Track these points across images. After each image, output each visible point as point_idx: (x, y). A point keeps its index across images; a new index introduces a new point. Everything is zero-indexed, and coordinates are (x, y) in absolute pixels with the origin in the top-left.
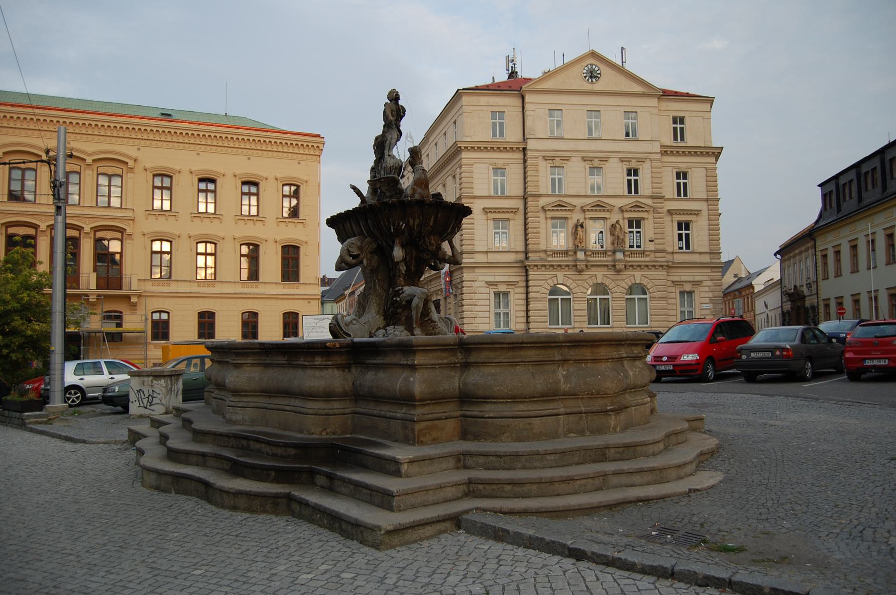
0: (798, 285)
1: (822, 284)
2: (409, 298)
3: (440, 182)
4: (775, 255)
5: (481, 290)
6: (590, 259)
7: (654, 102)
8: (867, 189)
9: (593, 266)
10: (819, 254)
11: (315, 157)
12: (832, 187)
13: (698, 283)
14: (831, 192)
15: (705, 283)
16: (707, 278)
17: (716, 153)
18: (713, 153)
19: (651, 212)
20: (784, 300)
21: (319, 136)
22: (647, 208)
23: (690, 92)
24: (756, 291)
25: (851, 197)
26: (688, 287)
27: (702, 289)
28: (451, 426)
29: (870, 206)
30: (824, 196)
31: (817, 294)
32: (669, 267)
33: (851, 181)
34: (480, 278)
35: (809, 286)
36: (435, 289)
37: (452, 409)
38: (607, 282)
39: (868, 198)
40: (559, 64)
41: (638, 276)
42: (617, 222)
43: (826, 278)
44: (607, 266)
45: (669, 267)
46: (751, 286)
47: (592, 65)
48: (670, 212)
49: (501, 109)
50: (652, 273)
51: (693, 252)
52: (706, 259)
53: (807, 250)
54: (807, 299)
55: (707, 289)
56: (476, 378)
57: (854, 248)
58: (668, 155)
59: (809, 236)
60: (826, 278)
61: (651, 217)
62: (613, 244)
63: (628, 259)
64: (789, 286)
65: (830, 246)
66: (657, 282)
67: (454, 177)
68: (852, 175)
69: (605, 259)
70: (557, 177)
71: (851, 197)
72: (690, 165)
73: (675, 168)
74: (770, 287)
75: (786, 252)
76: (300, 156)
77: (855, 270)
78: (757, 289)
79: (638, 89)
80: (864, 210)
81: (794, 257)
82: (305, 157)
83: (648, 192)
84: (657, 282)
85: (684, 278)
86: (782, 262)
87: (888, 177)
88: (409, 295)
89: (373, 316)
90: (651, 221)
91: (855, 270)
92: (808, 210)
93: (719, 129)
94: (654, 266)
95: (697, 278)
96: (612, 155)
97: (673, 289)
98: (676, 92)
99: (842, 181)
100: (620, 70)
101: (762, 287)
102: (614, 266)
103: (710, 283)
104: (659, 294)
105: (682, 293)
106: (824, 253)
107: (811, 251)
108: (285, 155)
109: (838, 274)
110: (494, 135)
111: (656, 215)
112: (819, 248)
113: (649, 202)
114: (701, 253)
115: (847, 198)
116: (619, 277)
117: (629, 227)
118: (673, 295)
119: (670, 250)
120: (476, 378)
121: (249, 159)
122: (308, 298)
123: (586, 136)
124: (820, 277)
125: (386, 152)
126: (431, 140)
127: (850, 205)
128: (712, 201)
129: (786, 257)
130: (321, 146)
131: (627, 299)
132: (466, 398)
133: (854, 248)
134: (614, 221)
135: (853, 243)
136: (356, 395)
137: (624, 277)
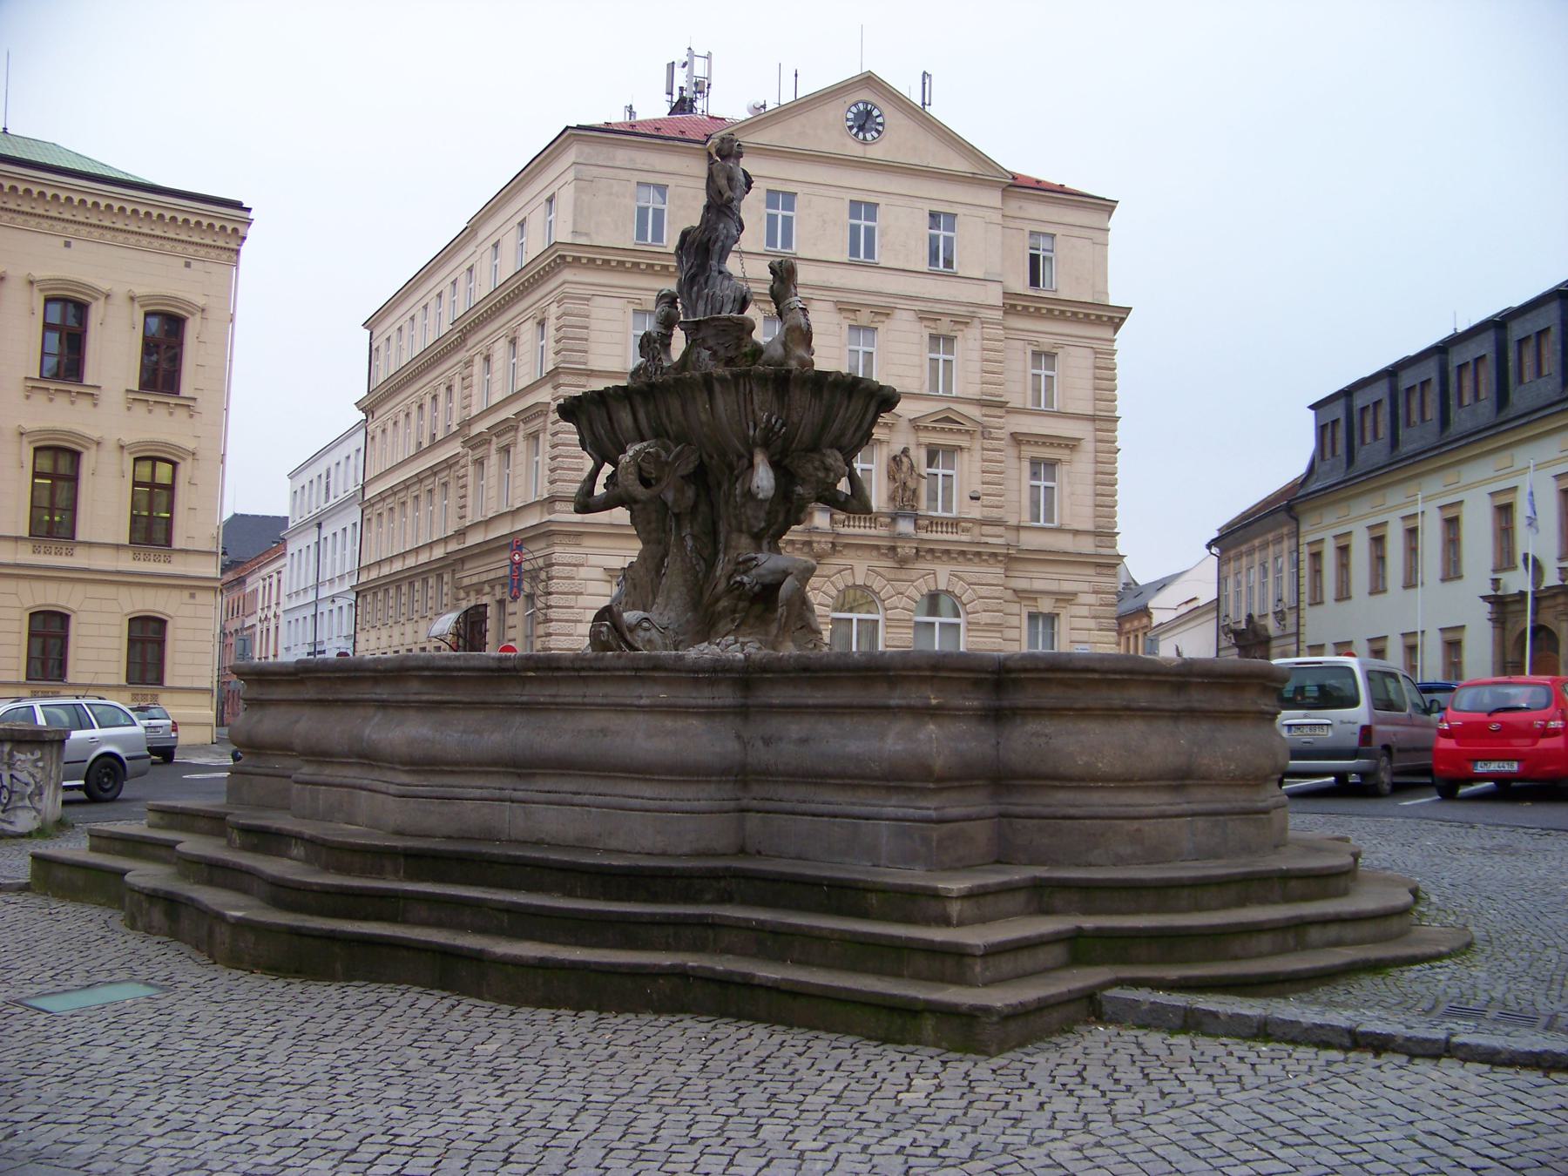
0: (1256, 613)
1: (1308, 613)
2: (768, 579)
3: (503, 332)
4: (1209, 546)
5: (593, 587)
6: (843, 530)
7: (993, 198)
8: (1408, 424)
9: (847, 546)
10: (1305, 552)
11: (225, 255)
12: (1338, 411)
13: (1067, 598)
14: (1335, 422)
15: (1083, 598)
16: (1085, 587)
17: (1115, 318)
18: (1111, 318)
19: (978, 435)
20: (1224, 644)
21: (238, 205)
22: (969, 426)
23: (1069, 185)
24: (1155, 623)
25: (1375, 436)
26: (1046, 606)
27: (1075, 610)
28: (981, 833)
29: (1418, 457)
30: (1321, 430)
31: (1298, 634)
32: (1011, 559)
33: (1377, 404)
34: (593, 560)
35: (1280, 616)
36: (475, 580)
37: (976, 803)
38: (877, 584)
39: (1412, 440)
40: (787, 98)
41: (943, 575)
42: (905, 451)
43: (1317, 601)
44: (877, 547)
45: (1011, 559)
46: (1145, 612)
47: (866, 103)
48: (1017, 439)
49: (872, 199)
50: (972, 571)
51: (1059, 530)
52: (1087, 545)
53: (1279, 540)
54: (1274, 643)
55: (1084, 611)
56: (1027, 741)
57: (1378, 541)
58: (1018, 314)
59: (1284, 510)
60: (1317, 601)
61: (977, 445)
62: (892, 498)
63: (923, 535)
64: (1237, 616)
65: (1328, 535)
66: (983, 591)
67: (541, 324)
68: (1381, 391)
69: (873, 532)
70: (862, 349)
71: (1375, 436)
72: (513, 324)
73: (1030, 342)
74: (1192, 614)
75: (1233, 540)
76: (191, 249)
77: (1378, 588)
78: (1158, 617)
79: (960, 165)
80: (1402, 464)
81: (1250, 553)
82: (203, 251)
83: (974, 391)
84: (983, 591)
85: (1038, 585)
86: (1222, 562)
87: (1453, 402)
88: (773, 572)
89: (667, 612)
90: (977, 455)
91: (1378, 588)
92: (1288, 454)
93: (1128, 268)
94: (979, 554)
95: (1067, 587)
96: (902, 304)
97: (1015, 608)
98: (1038, 182)
99: (1359, 401)
100: (919, 115)
101: (1172, 615)
102: (893, 549)
103: (1092, 599)
104: (985, 618)
105: (1033, 617)
106: (1315, 549)
107: (1287, 544)
108: (157, 243)
109: (1343, 595)
110: (642, 234)
111: (988, 443)
112: (1306, 538)
113: (974, 412)
114: (1076, 532)
115: (1368, 439)
116: (902, 574)
117: (929, 465)
118: (1014, 621)
119: (1013, 521)
120: (1027, 741)
121: (68, 245)
122: (191, 586)
123: (846, 258)
124: (1305, 598)
125: (714, 262)
126: (483, 234)
127: (1373, 451)
128: (1105, 421)
129: (1232, 553)
130: (241, 228)
131: (917, 623)
132: (1001, 779)
133: (1378, 541)
134: (897, 449)
135: (1377, 533)
136: (741, 775)
137: (914, 574)
